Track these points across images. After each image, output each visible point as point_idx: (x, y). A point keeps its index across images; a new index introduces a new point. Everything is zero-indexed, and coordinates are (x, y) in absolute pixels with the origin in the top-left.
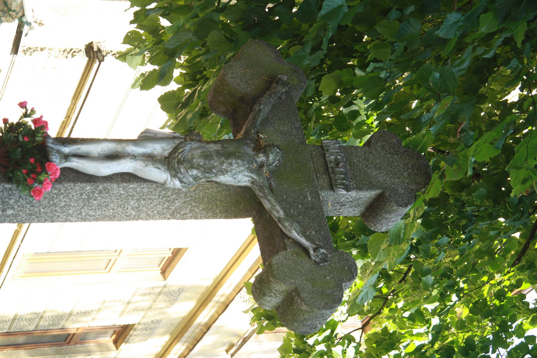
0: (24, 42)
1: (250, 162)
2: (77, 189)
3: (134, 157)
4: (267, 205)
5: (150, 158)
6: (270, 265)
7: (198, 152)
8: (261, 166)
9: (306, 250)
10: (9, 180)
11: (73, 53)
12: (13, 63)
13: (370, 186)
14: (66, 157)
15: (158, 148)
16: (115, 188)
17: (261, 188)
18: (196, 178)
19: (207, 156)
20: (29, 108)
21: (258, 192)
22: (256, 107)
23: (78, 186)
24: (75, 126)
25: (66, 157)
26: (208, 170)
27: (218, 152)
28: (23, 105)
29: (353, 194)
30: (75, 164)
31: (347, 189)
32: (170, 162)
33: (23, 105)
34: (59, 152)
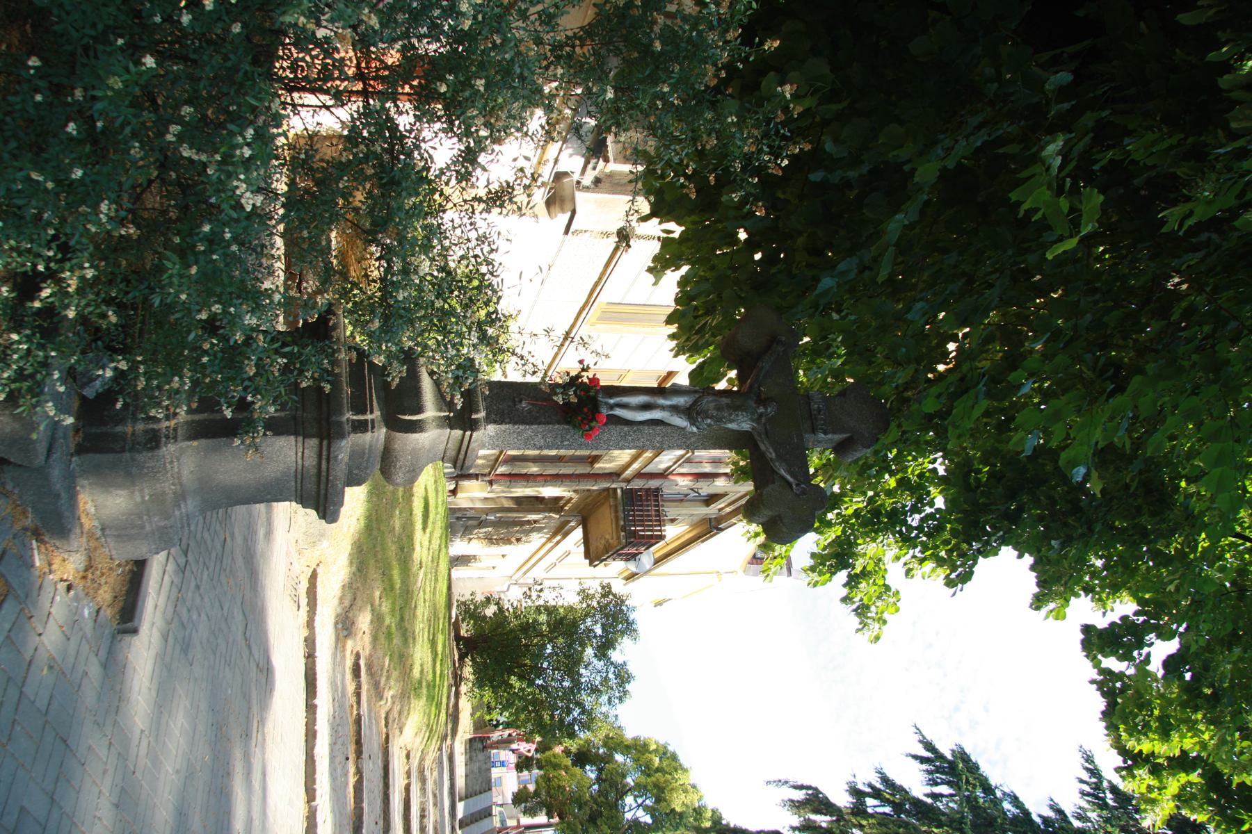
0: (573, 228)
1: (753, 414)
2: (617, 430)
3: (663, 408)
4: (763, 448)
5: (675, 409)
6: (761, 495)
7: (712, 405)
8: (761, 415)
9: (790, 484)
10: (568, 423)
11: (607, 235)
12: (564, 241)
13: (842, 431)
14: (612, 407)
15: (681, 401)
16: (646, 429)
17: (759, 434)
18: (709, 425)
19: (719, 408)
20: (585, 363)
21: (757, 437)
22: (759, 364)
23: (619, 428)
24: (601, 269)
25: (612, 407)
26: (718, 420)
27: (728, 405)
28: (581, 362)
29: (830, 436)
30: (619, 412)
31: (825, 433)
32: (689, 413)
33: (581, 362)
34: (606, 404)
